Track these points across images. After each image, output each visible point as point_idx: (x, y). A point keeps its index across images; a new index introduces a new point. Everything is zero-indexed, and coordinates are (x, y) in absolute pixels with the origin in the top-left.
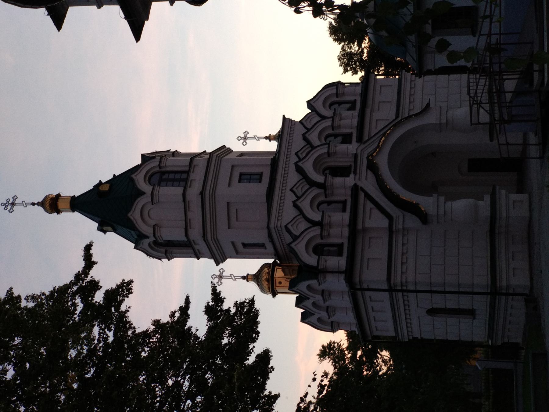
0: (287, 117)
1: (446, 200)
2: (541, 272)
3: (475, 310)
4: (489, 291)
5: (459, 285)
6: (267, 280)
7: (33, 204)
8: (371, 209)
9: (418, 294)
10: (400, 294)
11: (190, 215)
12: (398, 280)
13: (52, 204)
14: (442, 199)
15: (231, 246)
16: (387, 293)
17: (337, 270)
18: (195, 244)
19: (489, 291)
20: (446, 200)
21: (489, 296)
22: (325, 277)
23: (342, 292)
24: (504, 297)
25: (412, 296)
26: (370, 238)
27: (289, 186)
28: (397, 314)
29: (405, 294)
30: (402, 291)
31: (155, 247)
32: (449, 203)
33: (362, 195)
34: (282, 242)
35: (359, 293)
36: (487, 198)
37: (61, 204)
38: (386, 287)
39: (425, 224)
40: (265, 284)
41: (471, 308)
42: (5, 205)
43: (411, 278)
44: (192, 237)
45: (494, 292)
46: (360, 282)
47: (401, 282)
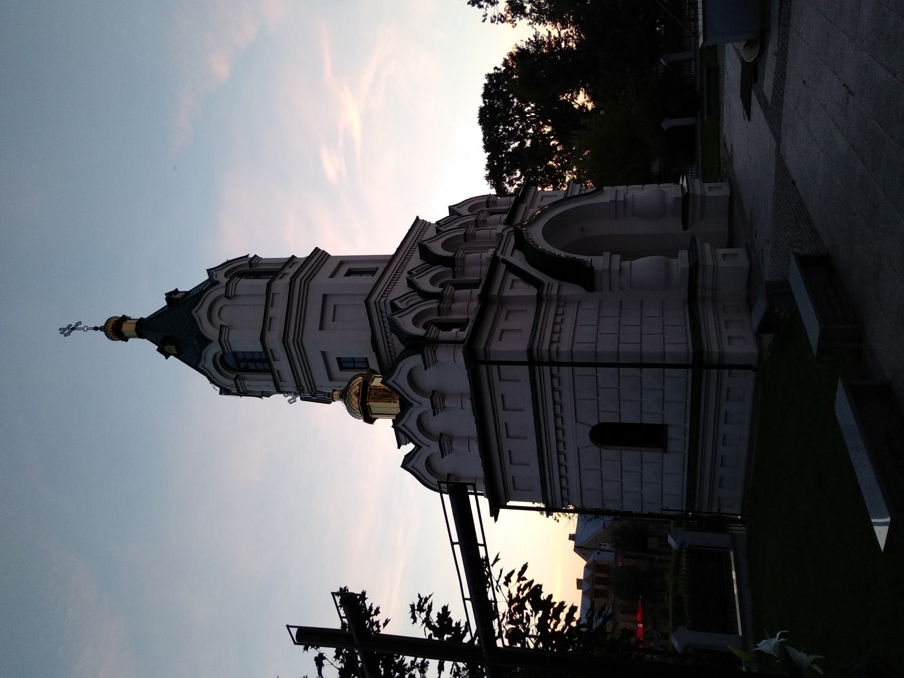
0: (421, 218)
1: (622, 259)
2: (793, 183)
3: (667, 425)
4: (691, 362)
5: (641, 355)
6: (357, 395)
7: (96, 329)
8: (513, 281)
9: (576, 368)
10: (547, 369)
11: (272, 312)
12: (545, 346)
13: (116, 329)
14: (617, 258)
15: (320, 355)
16: (527, 367)
17: (454, 339)
18: (274, 360)
19: (691, 362)
20: (622, 259)
21: (690, 370)
22: (435, 352)
23: (469, 438)
24: (714, 372)
25: (565, 371)
26: (508, 312)
27: (408, 268)
28: (545, 448)
29: (555, 369)
30: (551, 364)
31: (220, 365)
32: (626, 264)
33: (503, 267)
34: (387, 338)
35: (483, 368)
36: (684, 254)
37: (127, 328)
38: (525, 359)
39: (591, 291)
40: (355, 400)
41: (657, 421)
42: (62, 331)
43: (565, 347)
44: (270, 346)
45: (699, 363)
46: (485, 351)
47: (549, 350)
